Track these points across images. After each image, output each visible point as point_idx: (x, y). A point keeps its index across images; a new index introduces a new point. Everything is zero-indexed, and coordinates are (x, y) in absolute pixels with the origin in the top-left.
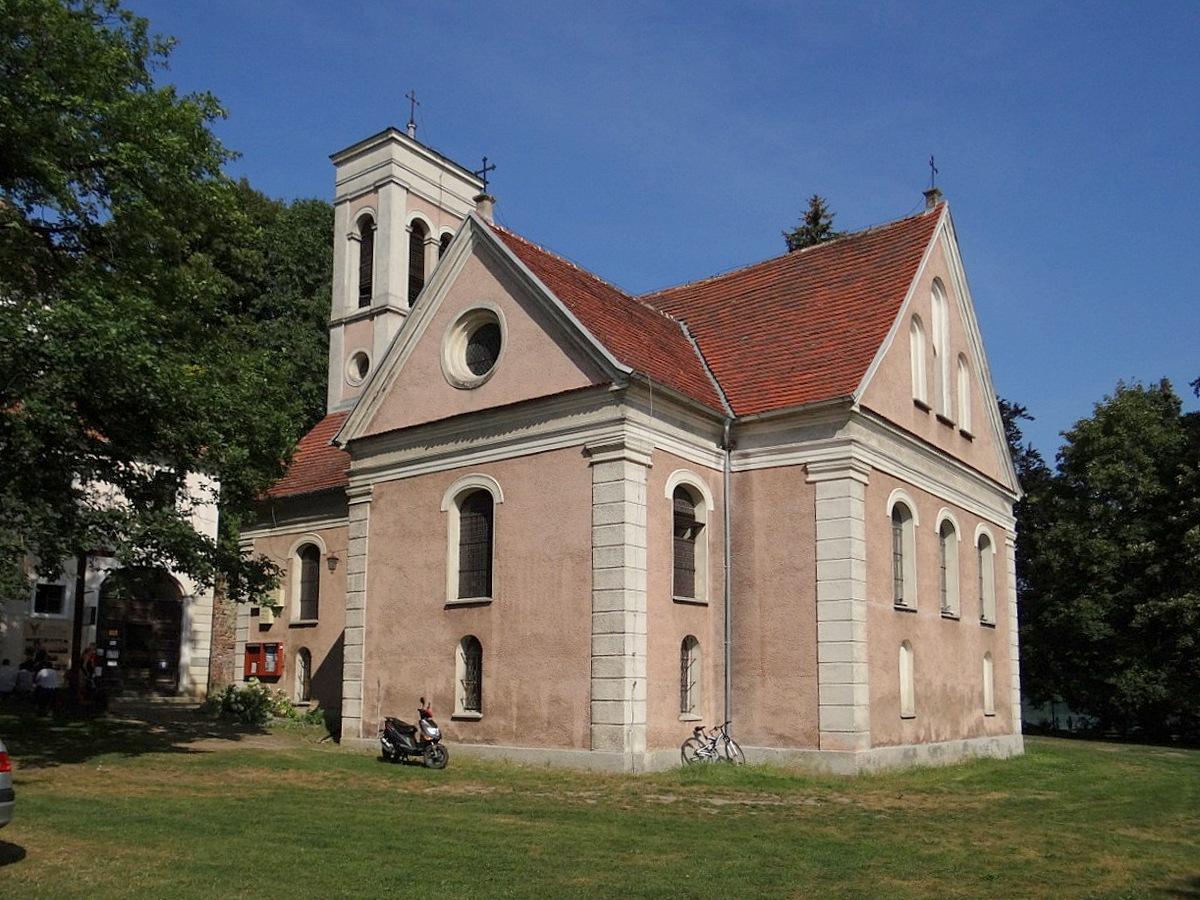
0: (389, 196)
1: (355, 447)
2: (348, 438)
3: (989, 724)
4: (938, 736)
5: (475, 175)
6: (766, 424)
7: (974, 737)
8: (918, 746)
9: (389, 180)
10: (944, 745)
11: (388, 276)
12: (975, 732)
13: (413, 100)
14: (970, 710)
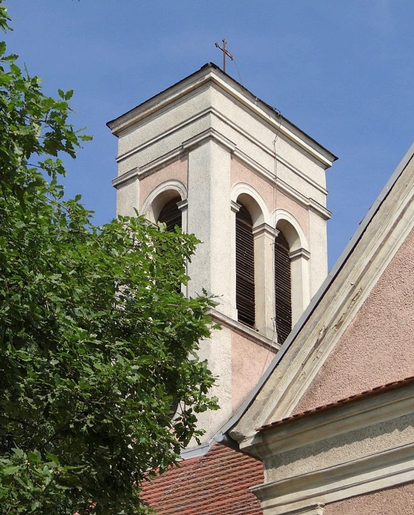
0: (206, 162)
1: (274, 442)
2: (260, 424)
9: (208, 136)
11: (208, 269)
13: (225, 52)
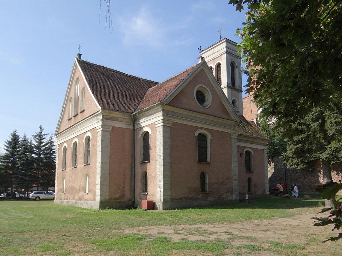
3: (86, 197)
4: (69, 199)
5: (221, 40)
6: (91, 149)
7: (79, 200)
8: (64, 201)
10: (70, 201)
12: (80, 199)
14: (79, 192)
